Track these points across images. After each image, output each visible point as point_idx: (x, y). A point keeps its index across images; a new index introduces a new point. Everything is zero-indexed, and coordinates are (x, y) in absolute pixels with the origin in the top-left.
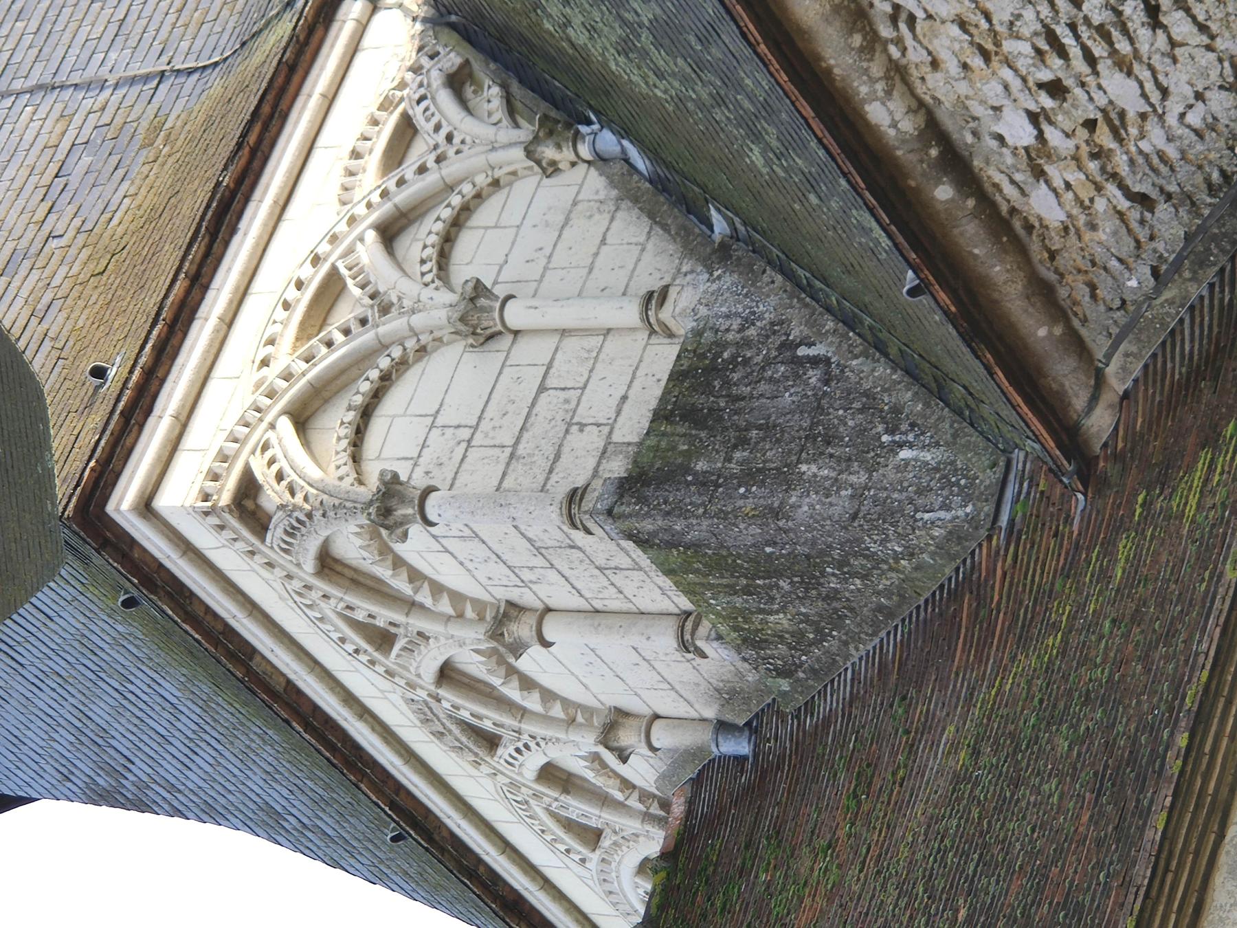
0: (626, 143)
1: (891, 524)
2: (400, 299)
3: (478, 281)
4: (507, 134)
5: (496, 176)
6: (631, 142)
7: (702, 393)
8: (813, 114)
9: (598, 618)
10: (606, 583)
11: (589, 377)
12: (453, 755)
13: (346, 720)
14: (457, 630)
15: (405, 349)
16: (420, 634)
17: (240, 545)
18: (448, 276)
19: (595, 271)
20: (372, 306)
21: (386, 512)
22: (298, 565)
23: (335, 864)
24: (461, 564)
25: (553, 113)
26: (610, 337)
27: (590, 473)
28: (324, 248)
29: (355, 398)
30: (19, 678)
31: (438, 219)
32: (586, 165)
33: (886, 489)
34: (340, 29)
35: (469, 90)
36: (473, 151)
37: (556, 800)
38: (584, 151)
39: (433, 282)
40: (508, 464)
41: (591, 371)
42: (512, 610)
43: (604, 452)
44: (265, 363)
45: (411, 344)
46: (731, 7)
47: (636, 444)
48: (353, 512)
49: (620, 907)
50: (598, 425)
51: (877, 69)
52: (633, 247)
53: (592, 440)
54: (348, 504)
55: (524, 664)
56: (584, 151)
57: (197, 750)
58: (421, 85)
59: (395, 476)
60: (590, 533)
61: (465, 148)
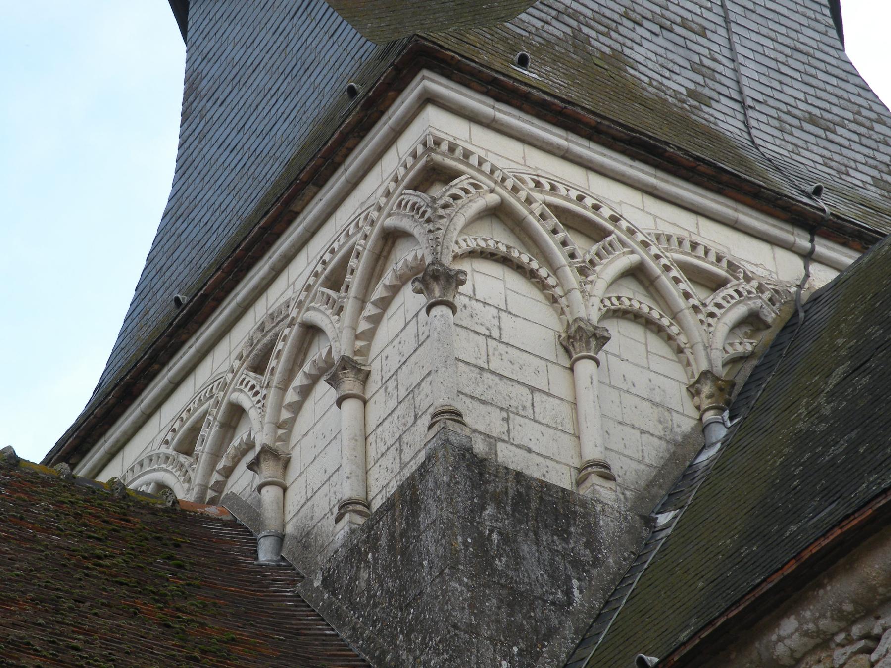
0: (719, 446)
1: (451, 656)
2: (591, 282)
3: (609, 339)
4: (718, 358)
5: (685, 350)
6: (720, 450)
7: (545, 509)
8: (785, 574)
9: (361, 440)
10: (389, 443)
11: (543, 424)
12: (247, 339)
13: (270, 258)
14: (346, 335)
15: (554, 287)
16: (341, 308)
17: (402, 171)
18: (609, 317)
19: (621, 427)
20: (584, 262)
21: (436, 277)
22: (389, 215)
23: (150, 260)
24: (397, 336)
25: (736, 391)
26: (573, 439)
27: (473, 427)
28: (624, 224)
29: (516, 251)
30: (282, 17)
31: (651, 309)
32: (698, 417)
33: (478, 652)
34: (787, 231)
35: (747, 329)
36: (703, 333)
37: (215, 419)
38: (709, 416)
39: (605, 306)
40: (475, 366)
41: (547, 425)
42: (365, 377)
43: (489, 436)
44: (538, 184)
45: (558, 291)
46: (870, 505)
47: (496, 460)
48: (434, 253)
49: (130, 472)
50: (508, 431)
51: (825, 624)
52: (640, 453)
53: (497, 428)
54: (439, 248)
55: (323, 386)
56: (709, 416)
57: (235, 152)
58: (749, 292)
59: (463, 283)
60: (430, 428)
61: (705, 327)
